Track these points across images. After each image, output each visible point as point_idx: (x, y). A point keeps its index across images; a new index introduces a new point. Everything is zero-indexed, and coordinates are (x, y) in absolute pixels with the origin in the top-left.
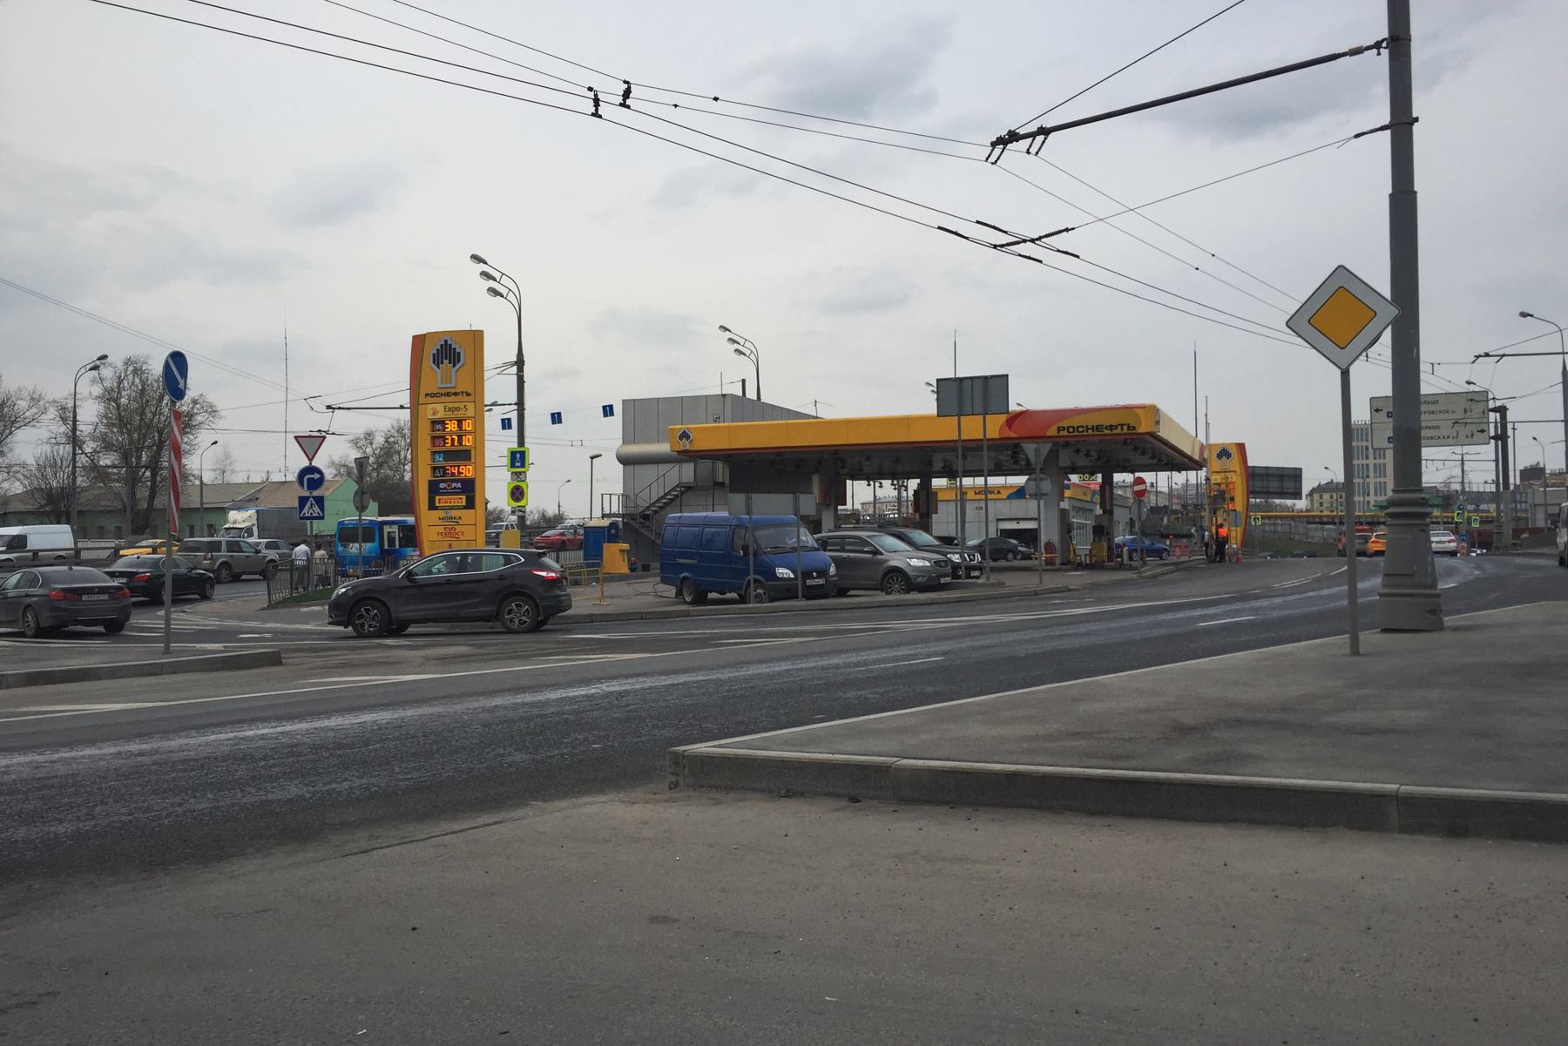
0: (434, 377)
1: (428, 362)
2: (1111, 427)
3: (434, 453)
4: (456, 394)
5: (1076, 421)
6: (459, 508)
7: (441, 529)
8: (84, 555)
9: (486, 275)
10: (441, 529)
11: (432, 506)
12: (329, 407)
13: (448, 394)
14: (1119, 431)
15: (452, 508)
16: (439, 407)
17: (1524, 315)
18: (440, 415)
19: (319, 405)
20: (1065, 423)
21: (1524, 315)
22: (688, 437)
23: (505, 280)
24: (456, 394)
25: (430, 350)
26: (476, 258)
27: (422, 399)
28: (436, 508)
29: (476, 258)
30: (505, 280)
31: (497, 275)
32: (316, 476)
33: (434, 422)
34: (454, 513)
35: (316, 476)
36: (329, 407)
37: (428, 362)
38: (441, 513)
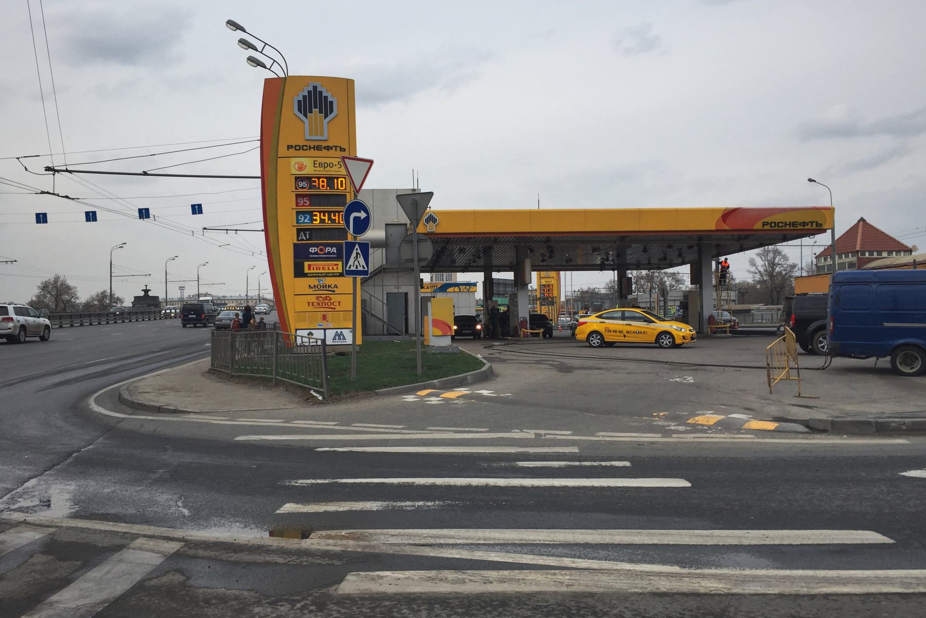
0: (295, 126)
1: (290, 109)
2: (804, 224)
3: (298, 213)
4: (328, 148)
5: (777, 218)
6: (334, 275)
7: (313, 299)
8: (627, 314)
9: (242, 42)
10: (313, 299)
11: (299, 272)
12: (48, 169)
13: (318, 148)
14: (809, 227)
15: (327, 275)
16: (305, 161)
17: (810, 180)
18: (309, 170)
19: (38, 166)
20: (769, 220)
21: (810, 180)
22: (434, 220)
23: (268, 50)
24: (328, 148)
25: (292, 98)
26: (233, 25)
27: (282, 151)
28: (306, 275)
29: (233, 25)
30: (268, 50)
31: (259, 46)
32: (362, 215)
33: (298, 179)
34: (328, 281)
35: (362, 215)
36: (48, 169)
37: (290, 109)
38: (313, 281)
